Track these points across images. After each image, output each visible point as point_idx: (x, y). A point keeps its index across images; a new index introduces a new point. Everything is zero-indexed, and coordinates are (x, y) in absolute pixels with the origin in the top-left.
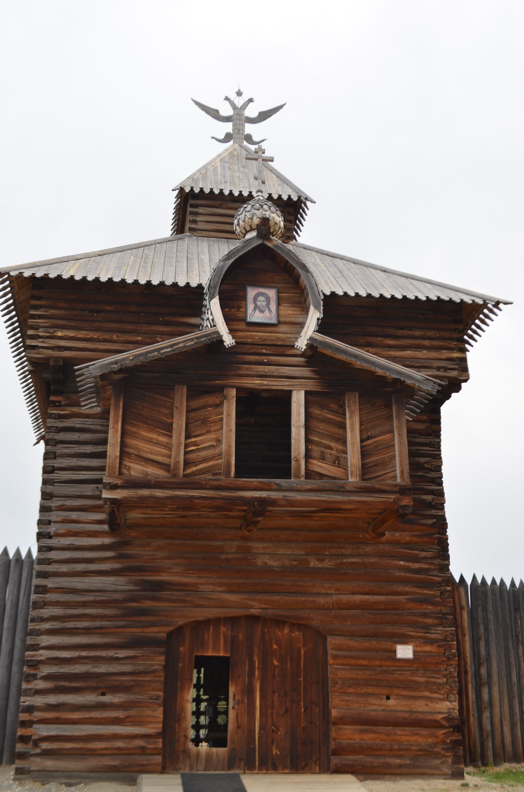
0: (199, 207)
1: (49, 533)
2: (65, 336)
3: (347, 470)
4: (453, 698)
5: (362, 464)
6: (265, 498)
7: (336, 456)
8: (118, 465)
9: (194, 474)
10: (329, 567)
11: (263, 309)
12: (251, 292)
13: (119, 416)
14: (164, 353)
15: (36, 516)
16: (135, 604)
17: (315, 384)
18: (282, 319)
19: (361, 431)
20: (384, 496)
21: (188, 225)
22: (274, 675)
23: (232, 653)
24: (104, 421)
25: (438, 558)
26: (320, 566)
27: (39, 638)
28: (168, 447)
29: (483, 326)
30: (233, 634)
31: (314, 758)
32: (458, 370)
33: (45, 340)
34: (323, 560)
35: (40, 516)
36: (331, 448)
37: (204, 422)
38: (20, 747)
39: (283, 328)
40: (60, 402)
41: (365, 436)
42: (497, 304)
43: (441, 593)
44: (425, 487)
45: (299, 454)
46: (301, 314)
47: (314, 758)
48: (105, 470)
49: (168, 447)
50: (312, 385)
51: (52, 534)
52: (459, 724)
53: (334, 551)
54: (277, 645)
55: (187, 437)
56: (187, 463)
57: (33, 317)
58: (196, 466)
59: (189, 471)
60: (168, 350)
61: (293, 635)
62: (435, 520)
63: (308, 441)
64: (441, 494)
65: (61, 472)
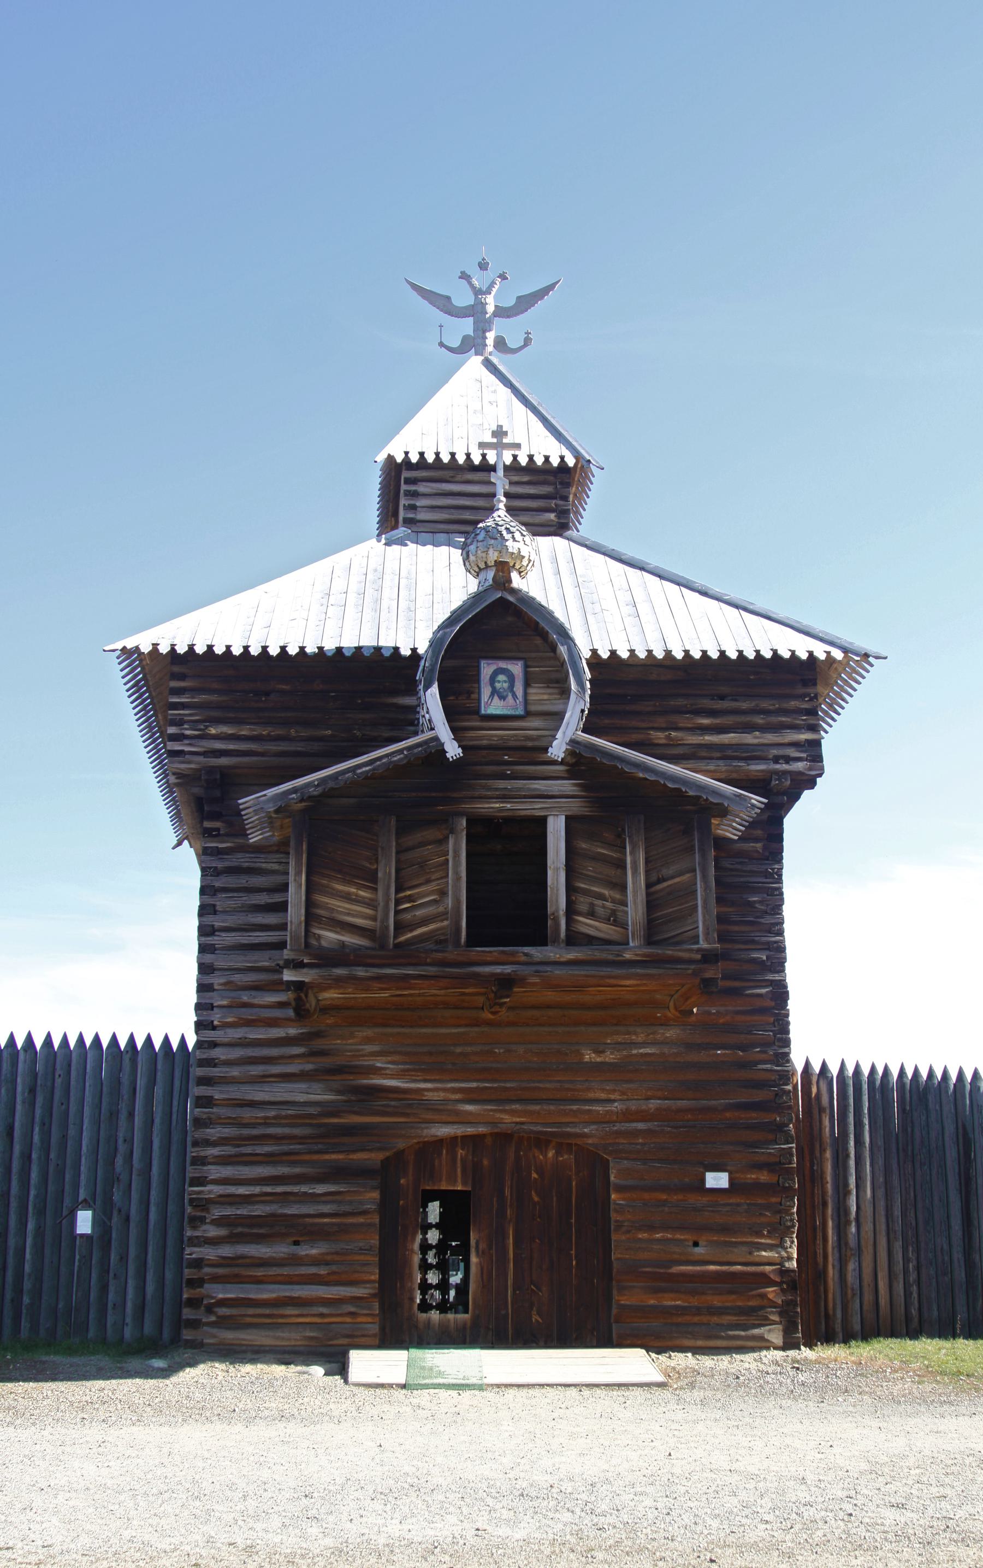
0: (419, 483)
2: (221, 733)
3: (627, 929)
6: (509, 974)
7: (612, 909)
8: (303, 934)
9: (409, 943)
10: (612, 1061)
11: (505, 694)
12: (487, 669)
13: (302, 863)
15: (193, 998)
16: (336, 1120)
17: (583, 804)
18: (533, 708)
19: (647, 872)
20: (679, 967)
21: (402, 514)
24: (282, 856)
26: (598, 1060)
27: (205, 1168)
28: (371, 904)
30: (475, 1159)
32: (806, 760)
33: (193, 741)
34: (603, 1052)
35: (198, 997)
37: (422, 866)
38: (187, 1313)
40: (218, 830)
41: (654, 878)
44: (756, 938)
45: (557, 910)
46: (560, 699)
48: (286, 929)
50: (576, 807)
51: (216, 1023)
53: (620, 1039)
54: (537, 1173)
55: (397, 892)
56: (400, 927)
57: (175, 706)
58: (411, 931)
59: (402, 939)
60: (368, 768)
61: (561, 1159)
63: (570, 889)
64: (781, 949)
65: (223, 934)
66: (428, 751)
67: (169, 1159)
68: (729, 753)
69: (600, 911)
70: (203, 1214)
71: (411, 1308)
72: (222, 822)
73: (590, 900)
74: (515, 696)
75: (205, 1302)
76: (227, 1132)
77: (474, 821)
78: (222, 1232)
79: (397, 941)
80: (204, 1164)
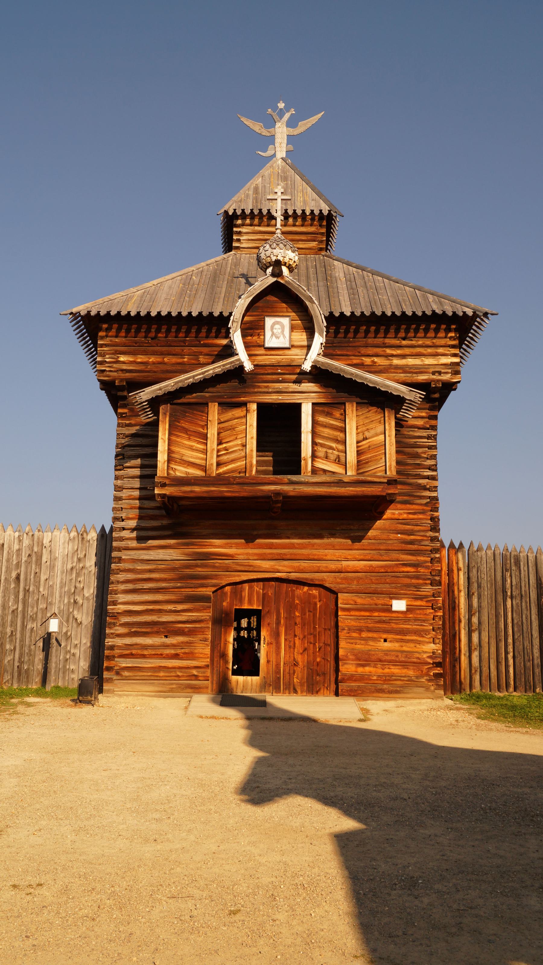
1: (122, 517)
4: (437, 641)
5: (357, 461)
8: (166, 468)
11: (279, 335)
12: (269, 321)
14: (197, 379)
18: (296, 344)
23: (263, 606)
25: (431, 531)
31: (326, 685)
36: (333, 449)
39: (294, 351)
43: (432, 559)
45: (307, 455)
47: (326, 685)
49: (205, 452)
52: (441, 661)
56: (219, 464)
58: (226, 466)
62: (429, 500)
63: (314, 443)
65: (129, 470)
66: (235, 366)
72: (128, 409)
73: (325, 450)
74: (284, 337)
75: (115, 668)
76: (130, 576)
78: (121, 630)
79: (217, 472)
80: (116, 594)
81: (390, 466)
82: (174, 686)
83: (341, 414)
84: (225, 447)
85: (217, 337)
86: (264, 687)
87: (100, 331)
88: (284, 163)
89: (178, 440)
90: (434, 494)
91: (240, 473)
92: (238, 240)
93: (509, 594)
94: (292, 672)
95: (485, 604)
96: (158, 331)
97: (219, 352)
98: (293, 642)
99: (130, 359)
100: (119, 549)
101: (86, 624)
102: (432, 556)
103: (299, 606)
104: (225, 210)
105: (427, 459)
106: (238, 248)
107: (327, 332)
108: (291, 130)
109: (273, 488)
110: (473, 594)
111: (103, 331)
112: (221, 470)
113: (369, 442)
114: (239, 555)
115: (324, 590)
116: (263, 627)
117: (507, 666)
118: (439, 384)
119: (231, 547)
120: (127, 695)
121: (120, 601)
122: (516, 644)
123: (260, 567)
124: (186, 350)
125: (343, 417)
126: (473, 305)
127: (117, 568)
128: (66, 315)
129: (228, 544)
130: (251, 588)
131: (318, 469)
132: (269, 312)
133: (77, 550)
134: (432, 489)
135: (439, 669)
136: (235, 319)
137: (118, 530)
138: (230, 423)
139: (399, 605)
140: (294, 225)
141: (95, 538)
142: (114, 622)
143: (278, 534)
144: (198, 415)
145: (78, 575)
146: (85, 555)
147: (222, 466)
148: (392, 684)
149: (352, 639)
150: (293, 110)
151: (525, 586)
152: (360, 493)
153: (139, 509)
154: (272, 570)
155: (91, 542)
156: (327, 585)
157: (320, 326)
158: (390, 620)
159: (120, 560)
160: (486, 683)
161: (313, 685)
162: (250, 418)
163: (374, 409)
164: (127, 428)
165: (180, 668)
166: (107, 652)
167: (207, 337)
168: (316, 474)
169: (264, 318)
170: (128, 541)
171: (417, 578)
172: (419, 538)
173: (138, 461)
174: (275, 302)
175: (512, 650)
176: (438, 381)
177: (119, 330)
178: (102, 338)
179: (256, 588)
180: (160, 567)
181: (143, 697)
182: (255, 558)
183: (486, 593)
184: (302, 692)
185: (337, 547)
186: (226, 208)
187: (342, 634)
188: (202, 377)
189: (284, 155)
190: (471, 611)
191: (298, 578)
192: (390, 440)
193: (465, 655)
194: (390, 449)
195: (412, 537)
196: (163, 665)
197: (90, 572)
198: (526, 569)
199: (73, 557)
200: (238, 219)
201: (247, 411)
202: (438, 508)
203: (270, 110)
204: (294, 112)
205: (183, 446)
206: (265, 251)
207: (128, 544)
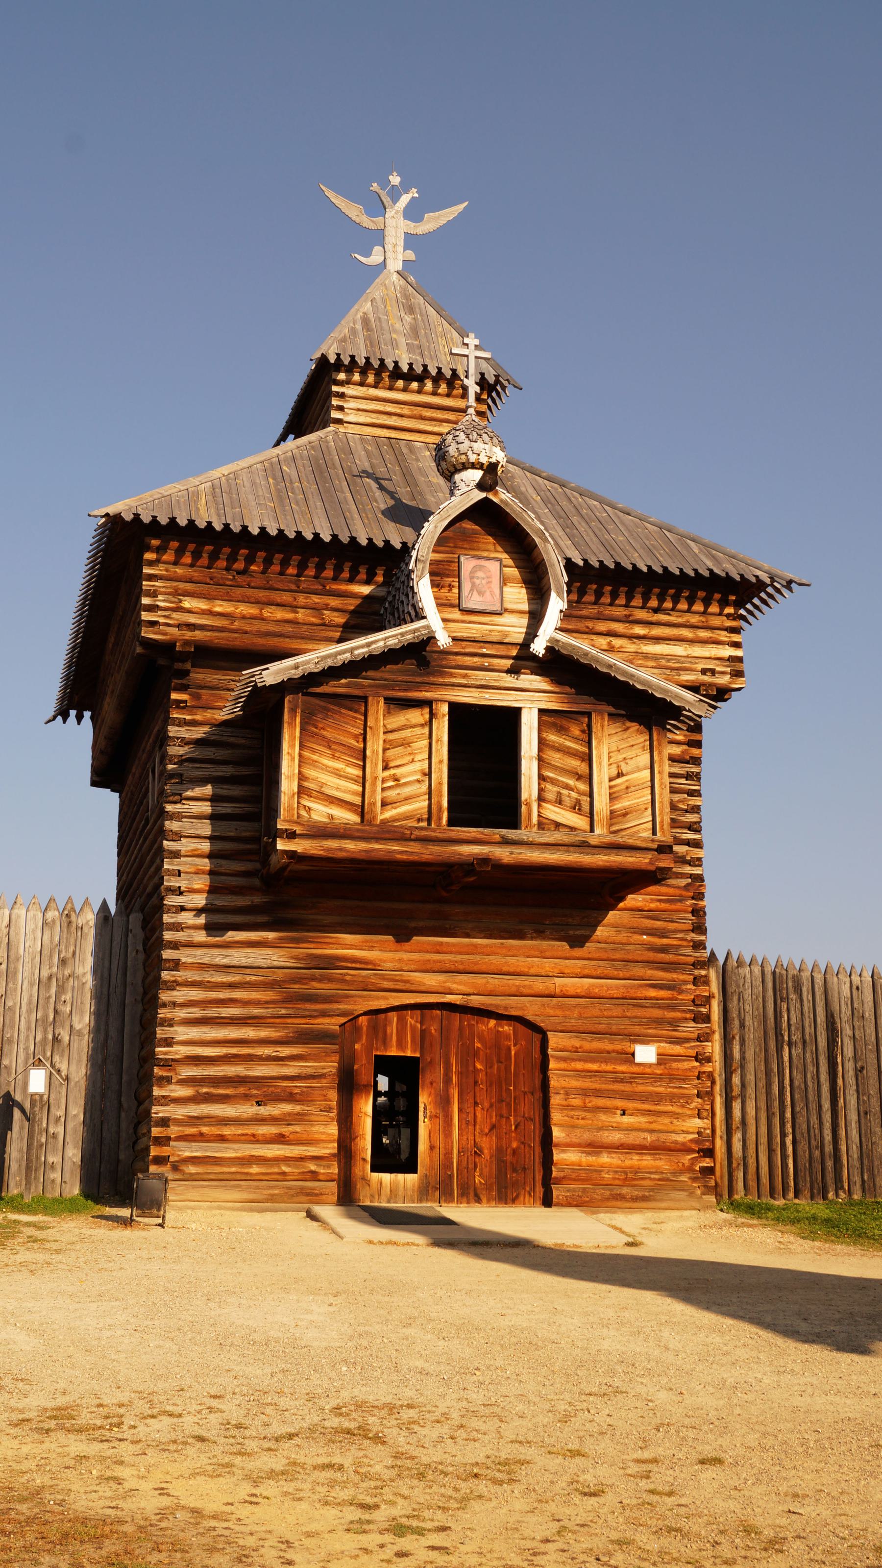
1: (180, 887)
8: (296, 806)
12: (467, 564)
18: (507, 605)
22: (476, 1082)
25: (693, 931)
29: (763, 607)
31: (528, 1189)
39: (507, 619)
40: (185, 702)
42: (789, 584)
43: (695, 978)
45: (530, 795)
56: (384, 804)
63: (542, 778)
65: (191, 803)
66: (421, 638)
67: (124, 1019)
68: (663, 662)
69: (567, 801)
70: (169, 1074)
71: (364, 1170)
72: (189, 694)
73: (555, 789)
75: (171, 1159)
77: (456, 709)
80: (171, 1026)
81: (662, 822)
82: (276, 1191)
83: (583, 731)
84: (394, 775)
85: (351, 580)
86: (424, 1192)
87: (147, 551)
88: (403, 282)
89: (315, 757)
90: (697, 871)
91: (419, 820)
92: (341, 408)
93: (786, 1038)
94: (471, 1166)
95: (750, 1054)
96: (250, 560)
97: (358, 606)
98: (472, 1115)
99: (202, 605)
100: (175, 945)
101: (77, 1080)
102: (696, 972)
103: (481, 1053)
104: (323, 354)
105: (687, 811)
106: (339, 421)
107: (569, 592)
108: (412, 224)
109: (476, 849)
110: (734, 1037)
111: (152, 552)
112: (389, 814)
113: (627, 781)
114: (385, 961)
115: (523, 1027)
116: (423, 1089)
117: (784, 1157)
118: (712, 691)
119: (371, 948)
120: (192, 1208)
121: (178, 1038)
122: (797, 1120)
123: (422, 984)
124: (302, 599)
125: (585, 737)
126: (766, 566)
127: (173, 979)
128: (96, 516)
129: (366, 941)
130: (402, 1021)
131: (547, 821)
132: (466, 549)
133: (59, 943)
134: (694, 862)
135: (708, 1160)
136: (419, 557)
137: (174, 910)
138: (406, 733)
139: (646, 1054)
140: (434, 393)
141: (92, 923)
142: (168, 1077)
143: (450, 929)
144: (349, 715)
145: (61, 989)
146: (74, 953)
147: (390, 807)
148: (636, 1185)
149: (572, 1110)
150: (415, 190)
151: (810, 1026)
152: (381, 856)
153: (209, 874)
154: (440, 990)
155: (85, 930)
156: (530, 1017)
157: (559, 581)
158: (631, 1078)
159: (176, 965)
160: (752, 1184)
161: (506, 1188)
162: (438, 728)
163: (635, 726)
164: (187, 728)
165: (286, 1160)
166: (156, 1131)
167: (335, 579)
168: (543, 829)
169: (459, 558)
170: (192, 931)
171: (673, 1008)
172: (675, 942)
173: (208, 790)
174: (475, 532)
175: (791, 1130)
176: (711, 685)
177: (180, 552)
178: (151, 563)
179: (410, 1021)
180: (249, 978)
181: (222, 1211)
182: (412, 967)
183: (752, 1036)
184: (489, 1201)
185: (548, 954)
186: (323, 350)
187: (555, 1100)
188: (366, 653)
189: (399, 266)
190: (731, 1066)
191: (483, 1004)
192: (661, 779)
193: (721, 1137)
194: (661, 794)
195: (665, 941)
196: (257, 1154)
197: (84, 984)
198: (810, 997)
199: (51, 957)
200: (339, 371)
201: (432, 715)
202: (703, 894)
203: (375, 185)
204: (416, 195)
205: (322, 769)
206: (458, 443)
207: (192, 936)
